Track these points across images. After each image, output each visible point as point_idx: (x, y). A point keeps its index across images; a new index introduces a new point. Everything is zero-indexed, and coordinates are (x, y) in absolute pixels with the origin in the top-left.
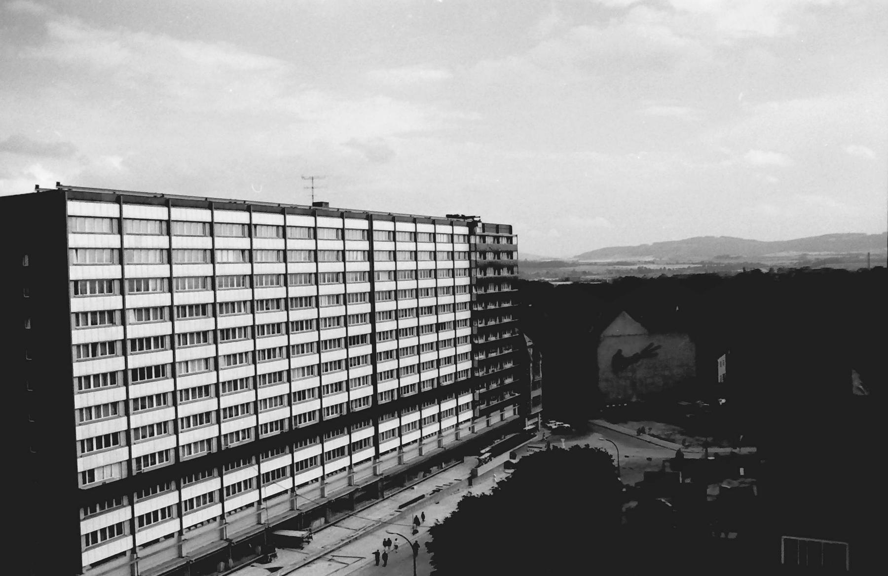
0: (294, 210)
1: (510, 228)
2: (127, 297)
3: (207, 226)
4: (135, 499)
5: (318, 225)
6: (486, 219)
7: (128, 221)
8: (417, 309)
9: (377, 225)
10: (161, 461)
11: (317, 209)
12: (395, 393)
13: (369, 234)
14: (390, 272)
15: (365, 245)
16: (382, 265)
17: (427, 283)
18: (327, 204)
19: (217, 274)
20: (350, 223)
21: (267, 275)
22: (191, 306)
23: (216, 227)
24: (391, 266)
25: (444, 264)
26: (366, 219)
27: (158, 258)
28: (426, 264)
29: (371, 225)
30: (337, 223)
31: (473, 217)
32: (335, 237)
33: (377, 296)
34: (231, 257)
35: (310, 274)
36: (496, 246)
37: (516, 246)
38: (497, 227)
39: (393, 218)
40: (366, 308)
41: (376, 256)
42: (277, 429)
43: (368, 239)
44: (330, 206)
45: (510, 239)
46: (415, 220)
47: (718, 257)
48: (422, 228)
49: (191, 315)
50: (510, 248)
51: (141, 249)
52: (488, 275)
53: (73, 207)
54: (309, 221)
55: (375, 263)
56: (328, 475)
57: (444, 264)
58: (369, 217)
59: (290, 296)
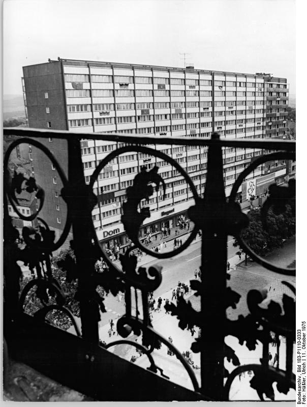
0: (175, 70)
1: (285, 80)
2: (94, 113)
3: (197, 81)
4: (101, 205)
5: (135, 75)
6: (275, 75)
7: (93, 76)
8: (254, 119)
9: (216, 78)
10: (112, 188)
11: (190, 69)
12: (253, 154)
13: (212, 82)
14: (222, 102)
15: (210, 88)
16: (218, 98)
17: (240, 108)
18: (193, 67)
19: (137, 102)
20: (202, 77)
21: (191, 102)
22: (124, 117)
23: (136, 79)
24: (223, 99)
25: (250, 98)
26: (211, 75)
27: (108, 94)
28: (241, 98)
29: (213, 78)
30: (196, 77)
31: (269, 74)
32: (208, 85)
33: (215, 114)
34: (143, 93)
35: (196, 102)
36: (278, 90)
37: (288, 90)
38: (279, 80)
39: (225, 74)
40: (210, 119)
41: (215, 94)
42: (165, 176)
43: (212, 85)
44: (195, 68)
45: (285, 86)
46: (236, 76)
47: (23, 91)
48: (240, 79)
49: (125, 121)
50: (285, 90)
51: (100, 90)
52: (280, 104)
53: (67, 69)
54: (182, 76)
55: (215, 98)
56: (105, 226)
57: (250, 98)
58: (212, 74)
59: (156, 114)
